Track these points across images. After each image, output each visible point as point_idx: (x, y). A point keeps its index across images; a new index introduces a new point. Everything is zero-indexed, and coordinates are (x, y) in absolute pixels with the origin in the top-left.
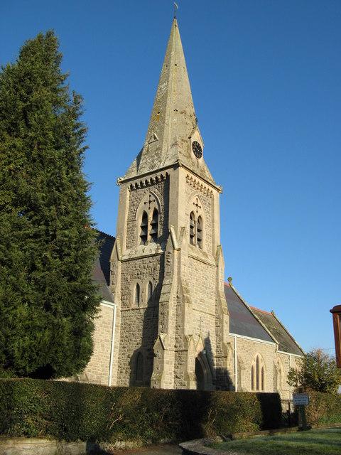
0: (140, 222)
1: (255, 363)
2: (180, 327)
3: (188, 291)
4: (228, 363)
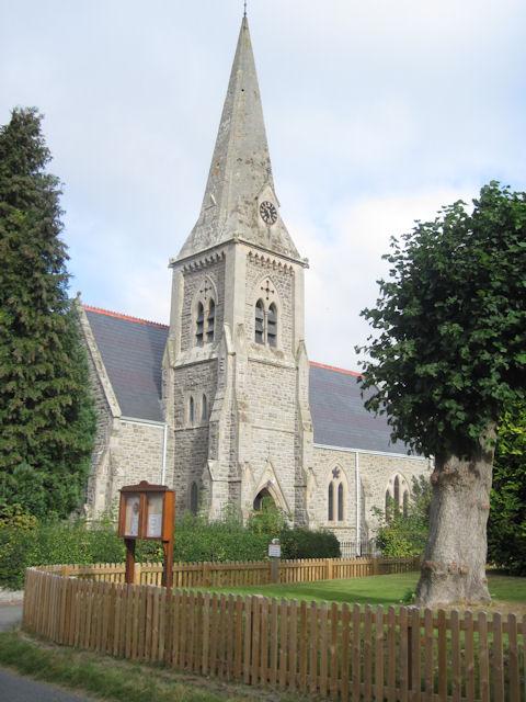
0: (195, 317)
1: (391, 488)
2: (233, 453)
3: (245, 406)
4: (308, 494)
